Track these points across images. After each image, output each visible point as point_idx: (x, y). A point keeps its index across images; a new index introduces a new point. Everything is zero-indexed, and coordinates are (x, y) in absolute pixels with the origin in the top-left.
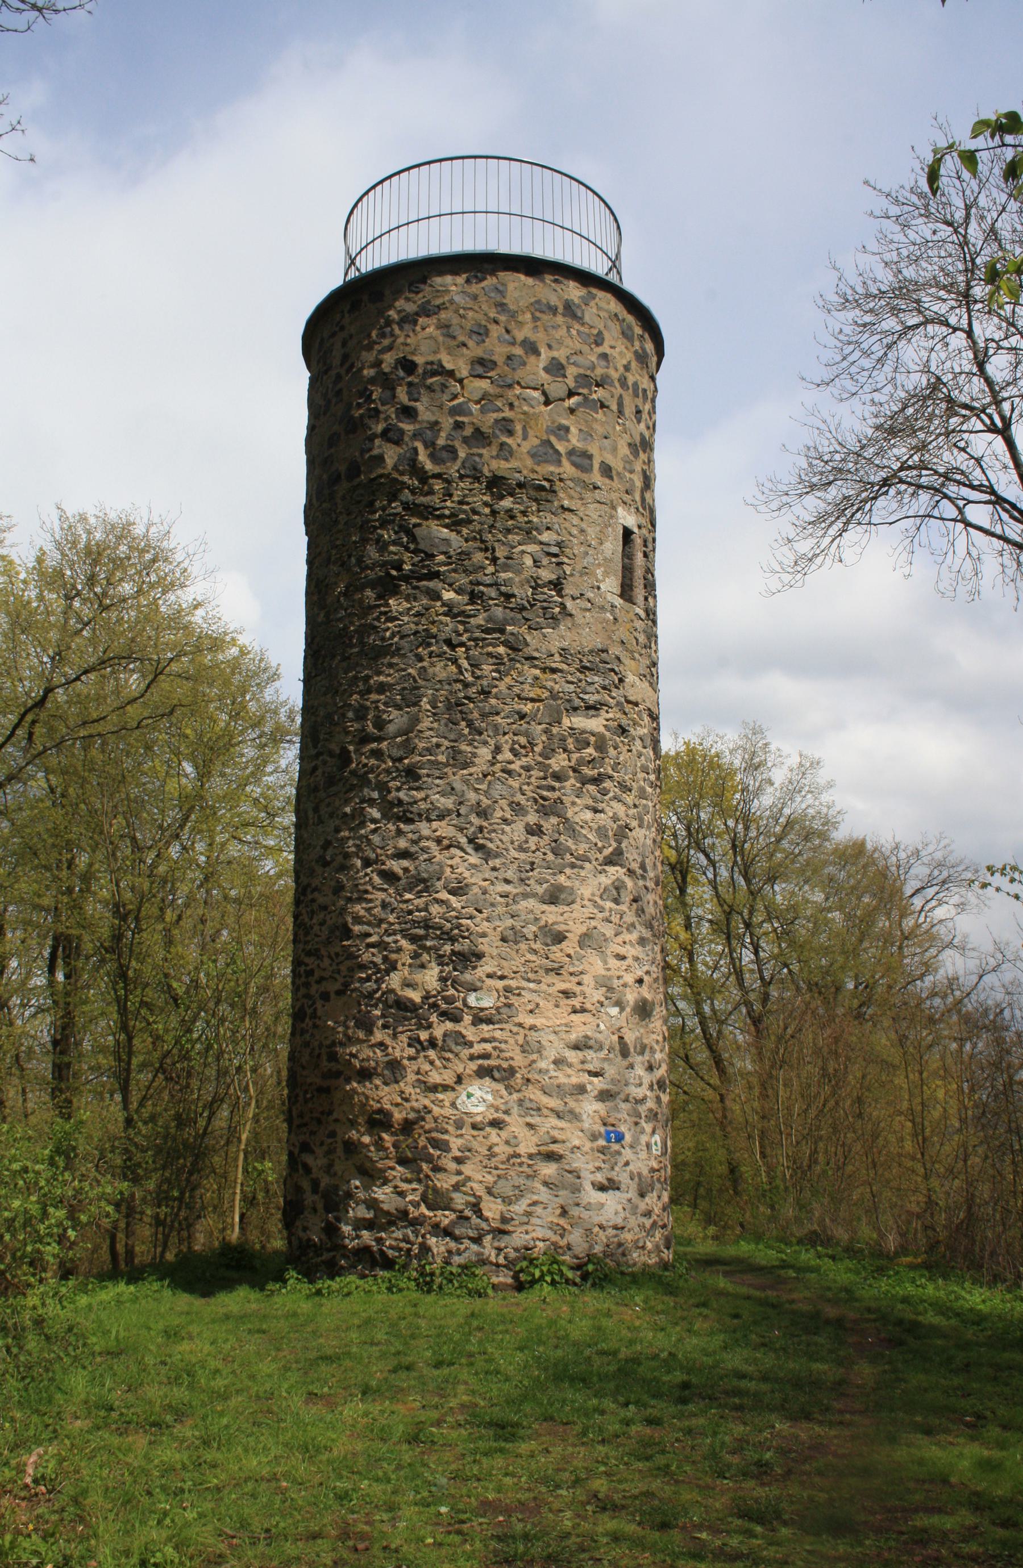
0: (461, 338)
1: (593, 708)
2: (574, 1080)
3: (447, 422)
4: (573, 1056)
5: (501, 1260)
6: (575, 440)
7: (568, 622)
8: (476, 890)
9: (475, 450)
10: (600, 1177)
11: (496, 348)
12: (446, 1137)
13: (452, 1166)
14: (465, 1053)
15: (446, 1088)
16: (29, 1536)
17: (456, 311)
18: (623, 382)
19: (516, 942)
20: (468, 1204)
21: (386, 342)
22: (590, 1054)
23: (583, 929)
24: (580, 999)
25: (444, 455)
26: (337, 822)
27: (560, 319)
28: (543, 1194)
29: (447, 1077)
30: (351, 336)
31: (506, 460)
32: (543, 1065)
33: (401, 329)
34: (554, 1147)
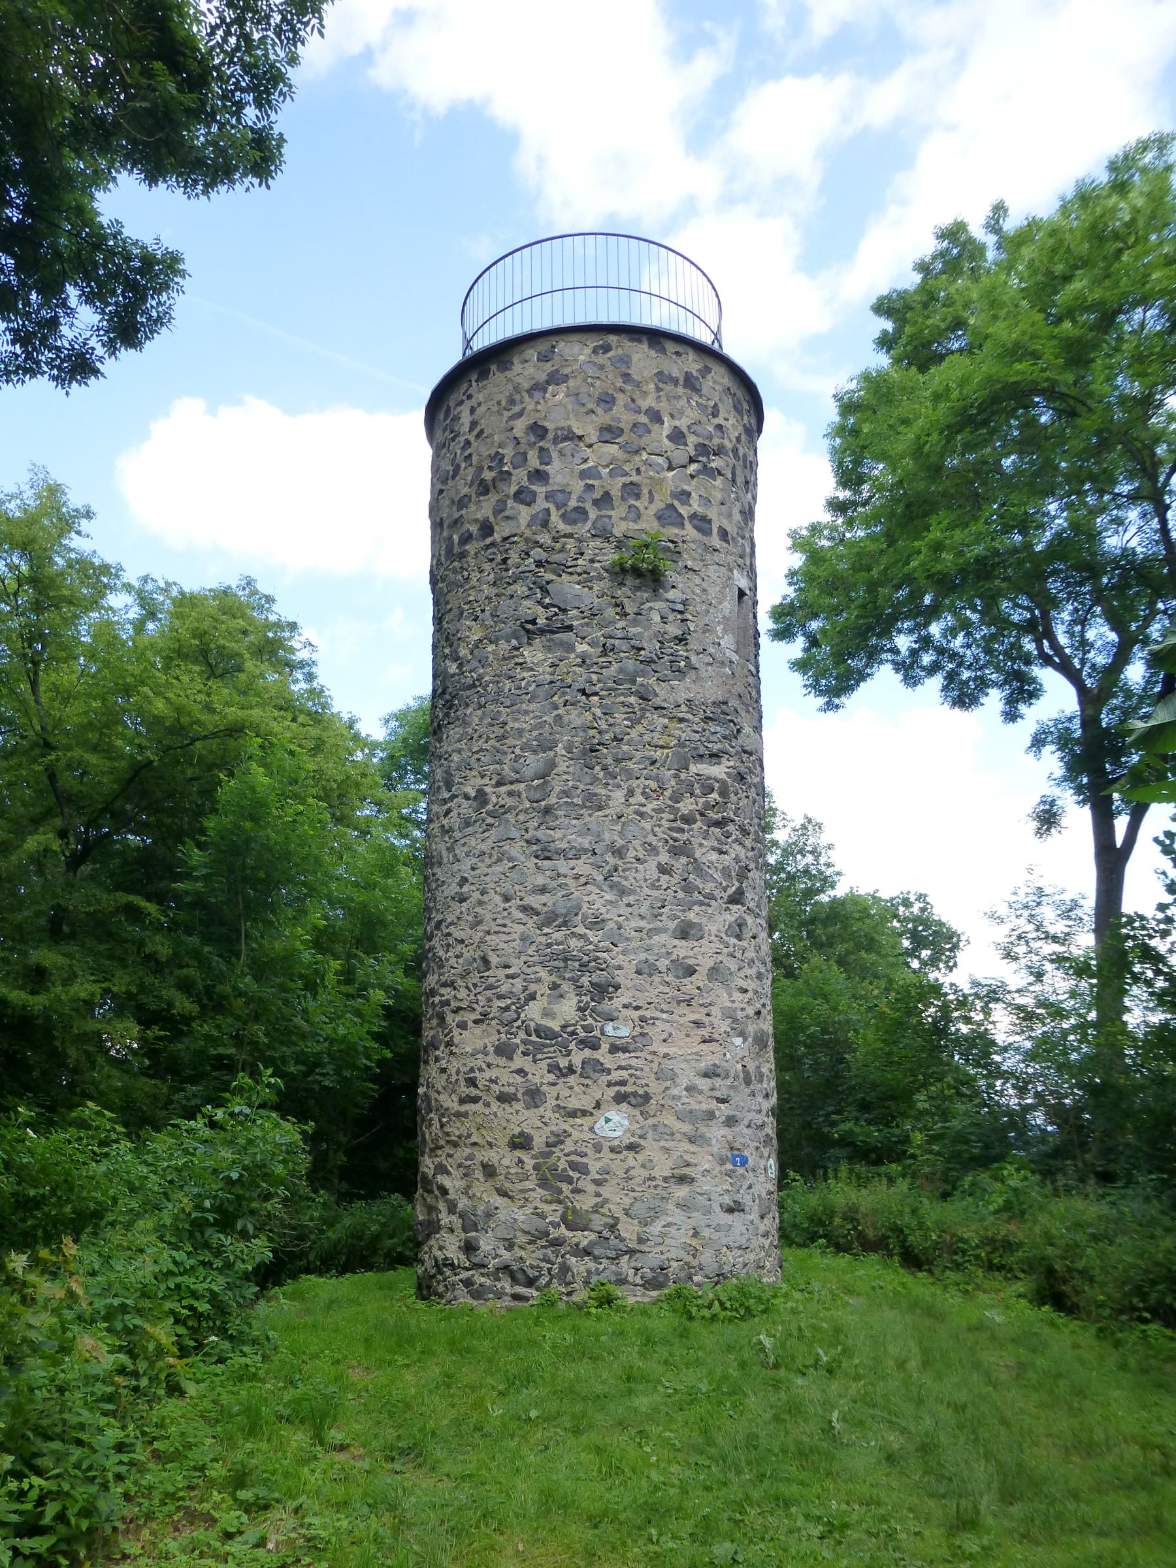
0: (590, 406)
1: (715, 756)
2: (704, 1107)
3: (578, 486)
4: (704, 1084)
5: (638, 1281)
6: (696, 506)
7: (692, 675)
8: (611, 925)
9: (604, 512)
10: (727, 1200)
11: (621, 415)
12: (584, 1160)
13: (591, 1188)
14: (605, 1079)
15: (584, 1113)
17: (585, 380)
18: (735, 451)
19: (651, 975)
20: (605, 1225)
21: (517, 409)
22: (718, 1082)
23: (711, 963)
24: (709, 1029)
25: (575, 515)
26: (474, 860)
27: (680, 390)
28: (677, 1216)
29: (587, 1103)
30: (479, 404)
31: (635, 521)
32: (675, 1091)
33: (531, 396)
34: (686, 1171)
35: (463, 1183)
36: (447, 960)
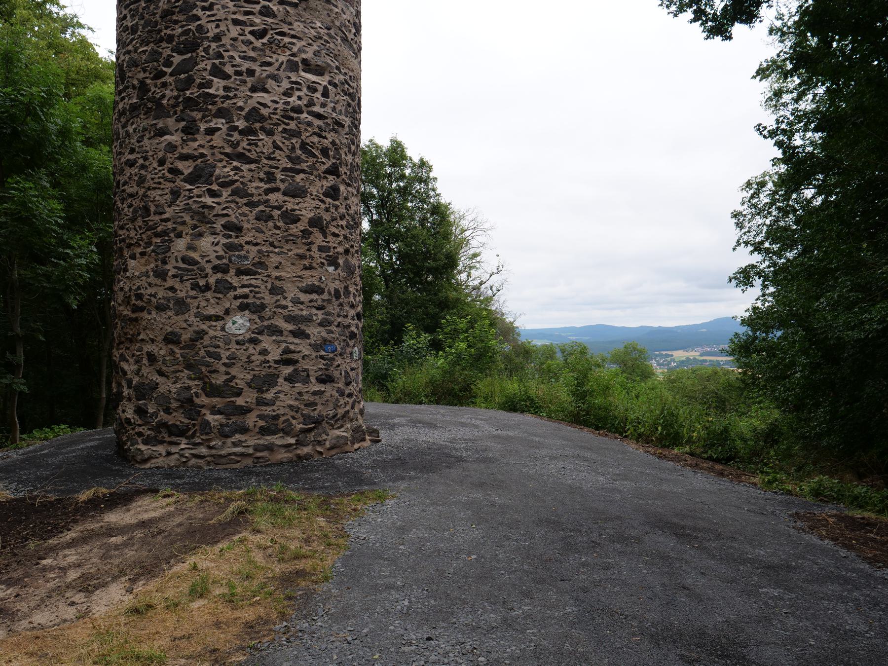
4: (304, 297)
13: (223, 369)
15: (218, 318)
16: (261, 264)
29: (218, 310)
34: (291, 356)
35: (136, 367)
36: (123, 210)
